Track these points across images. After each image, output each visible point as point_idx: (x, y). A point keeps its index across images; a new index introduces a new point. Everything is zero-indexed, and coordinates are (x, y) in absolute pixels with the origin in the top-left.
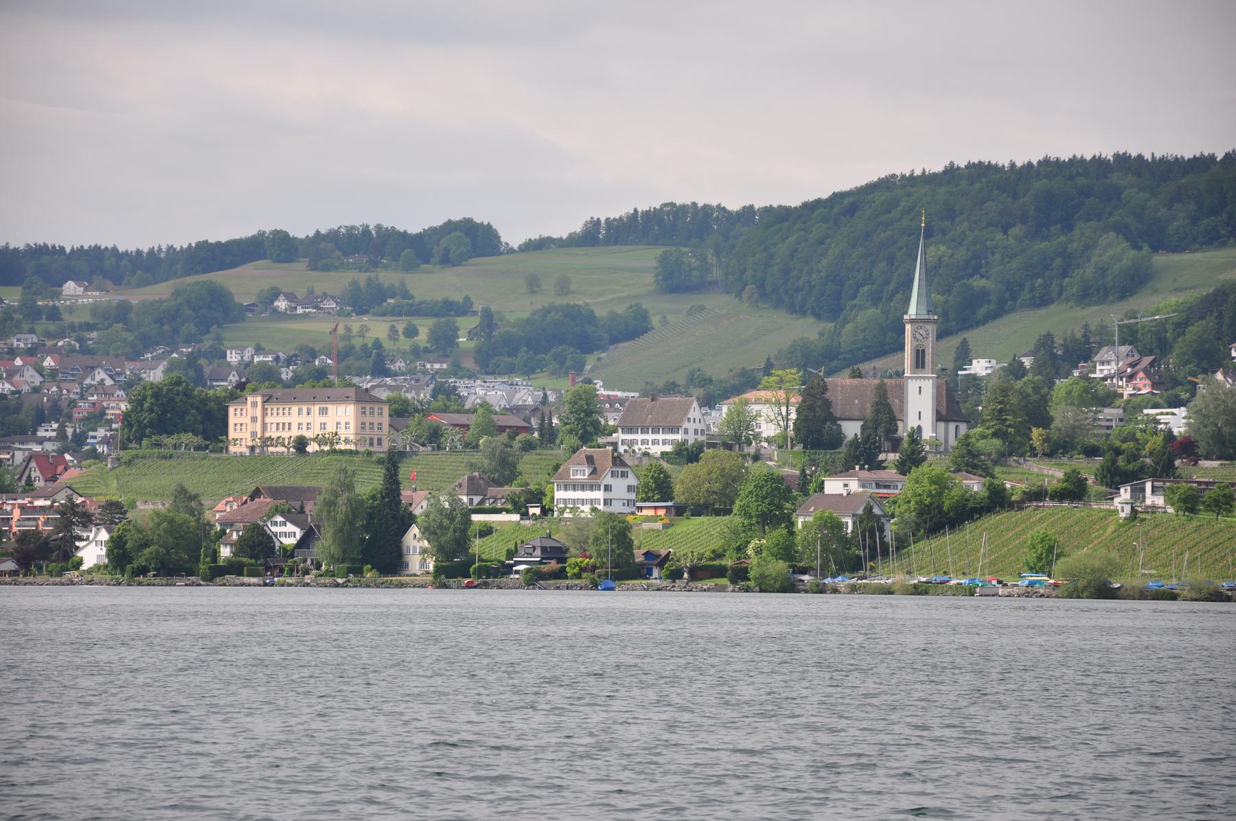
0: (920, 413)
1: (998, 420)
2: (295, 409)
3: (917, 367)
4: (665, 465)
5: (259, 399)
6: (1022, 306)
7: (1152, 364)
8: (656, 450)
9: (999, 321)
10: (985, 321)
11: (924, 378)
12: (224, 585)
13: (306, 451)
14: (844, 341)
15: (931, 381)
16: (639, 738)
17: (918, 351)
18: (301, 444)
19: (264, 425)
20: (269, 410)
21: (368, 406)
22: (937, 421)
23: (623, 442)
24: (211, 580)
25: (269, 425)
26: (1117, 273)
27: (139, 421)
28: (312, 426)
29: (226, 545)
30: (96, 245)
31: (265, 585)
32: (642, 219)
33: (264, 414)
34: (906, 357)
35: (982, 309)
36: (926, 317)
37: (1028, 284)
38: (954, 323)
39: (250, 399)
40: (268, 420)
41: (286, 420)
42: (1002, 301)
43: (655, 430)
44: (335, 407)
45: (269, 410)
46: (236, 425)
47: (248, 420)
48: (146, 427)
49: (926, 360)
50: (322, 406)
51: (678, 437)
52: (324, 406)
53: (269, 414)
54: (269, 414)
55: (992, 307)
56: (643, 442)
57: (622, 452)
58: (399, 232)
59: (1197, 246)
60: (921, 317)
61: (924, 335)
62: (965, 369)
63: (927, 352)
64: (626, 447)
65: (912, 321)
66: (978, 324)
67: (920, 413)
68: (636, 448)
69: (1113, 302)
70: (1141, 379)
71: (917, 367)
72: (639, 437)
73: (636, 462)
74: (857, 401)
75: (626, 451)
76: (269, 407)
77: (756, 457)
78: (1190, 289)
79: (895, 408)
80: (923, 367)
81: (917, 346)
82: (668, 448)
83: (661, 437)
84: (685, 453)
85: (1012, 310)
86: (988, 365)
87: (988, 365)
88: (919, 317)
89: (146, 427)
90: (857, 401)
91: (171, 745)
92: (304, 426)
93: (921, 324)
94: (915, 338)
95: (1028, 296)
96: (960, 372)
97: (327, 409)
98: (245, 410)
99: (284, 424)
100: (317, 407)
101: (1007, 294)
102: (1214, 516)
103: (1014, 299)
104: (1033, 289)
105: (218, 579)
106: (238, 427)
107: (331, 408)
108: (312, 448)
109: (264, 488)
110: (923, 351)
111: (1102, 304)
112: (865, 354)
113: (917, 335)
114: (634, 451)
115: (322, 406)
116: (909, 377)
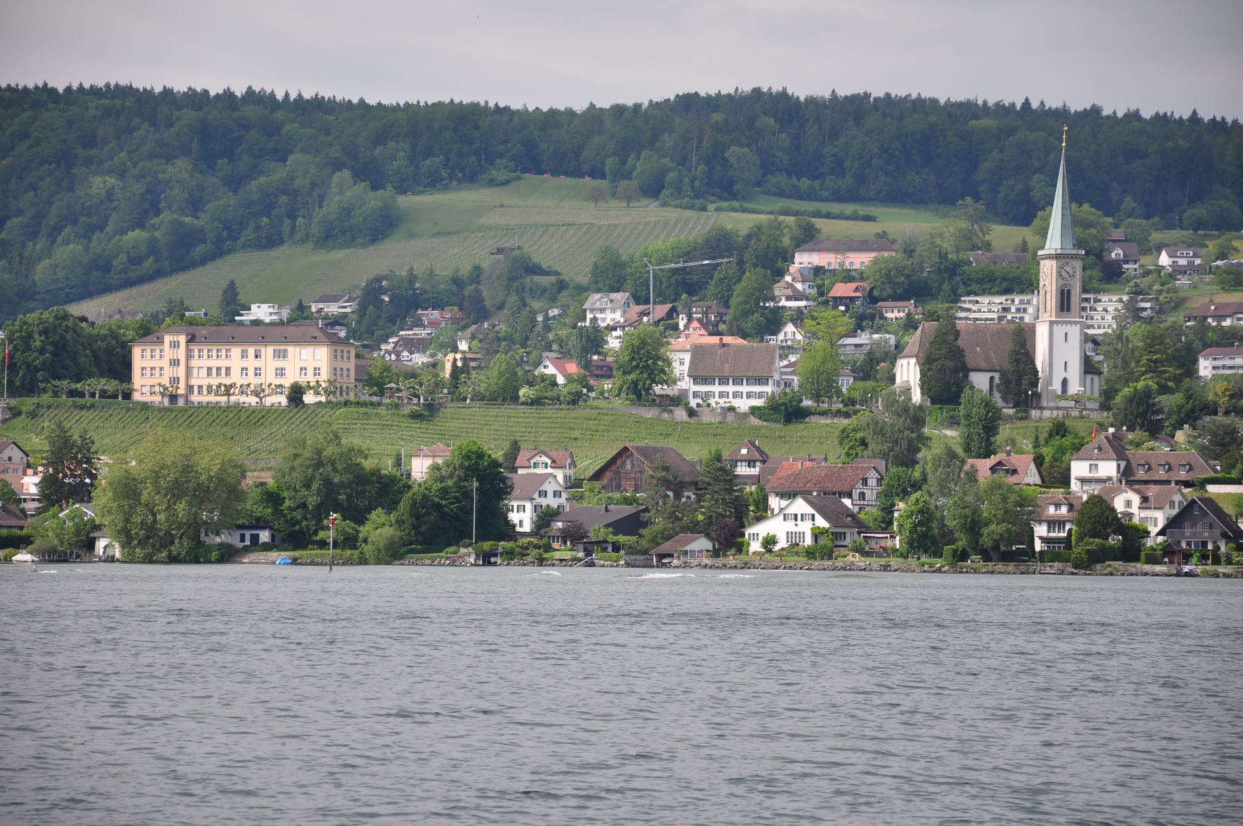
1: (1154, 372)
2: (236, 351)
3: (1062, 310)
4: (755, 421)
5: (182, 339)
6: (244, 246)
8: (743, 405)
9: (219, 262)
10: (203, 262)
11: (1071, 323)
12: (1111, 574)
13: (305, 405)
14: (40, 280)
16: (875, 709)
17: (1062, 291)
18: (296, 394)
19: (189, 369)
20: (196, 351)
21: (339, 349)
23: (695, 395)
24: (1087, 567)
25: (195, 371)
26: (368, 213)
27: (27, 363)
28: (263, 372)
29: (1040, 522)
31: (1178, 574)
33: (189, 356)
35: (198, 249)
36: (1074, 252)
37: (252, 223)
38: (167, 264)
39: (167, 339)
40: (195, 363)
41: (223, 363)
42: (219, 241)
43: (739, 381)
44: (297, 349)
45: (196, 351)
46: (143, 369)
47: (165, 363)
48: (37, 370)
49: (1072, 302)
50: (277, 348)
51: (768, 389)
52: (282, 348)
53: (196, 356)
54: (196, 356)
55: (210, 246)
56: (721, 395)
57: (695, 406)
58: (1080, 112)
59: (421, 188)
61: (1071, 273)
62: (242, 315)
63: (1073, 293)
64: (700, 401)
66: (194, 265)
68: (712, 402)
69: (363, 246)
70: (695, 329)
72: (716, 388)
73: (718, 419)
74: (978, 349)
75: (698, 405)
76: (195, 349)
78: (454, 233)
80: (1069, 310)
82: (759, 402)
83: (744, 389)
84: (783, 408)
85: (229, 252)
86: (271, 310)
87: (271, 310)
89: (37, 370)
90: (978, 349)
91: (479, 741)
92: (251, 372)
94: (1060, 276)
95: (253, 236)
96: (236, 318)
97: (285, 351)
98: (158, 351)
99: (219, 369)
100: (270, 349)
101: (225, 234)
103: (235, 239)
104: (258, 228)
105: (1098, 566)
106: (148, 372)
107: (292, 350)
108: (309, 398)
109: (637, 448)
110: (1069, 291)
111: (349, 247)
112: (68, 294)
113: (1064, 273)
114: (709, 405)
115: (277, 348)
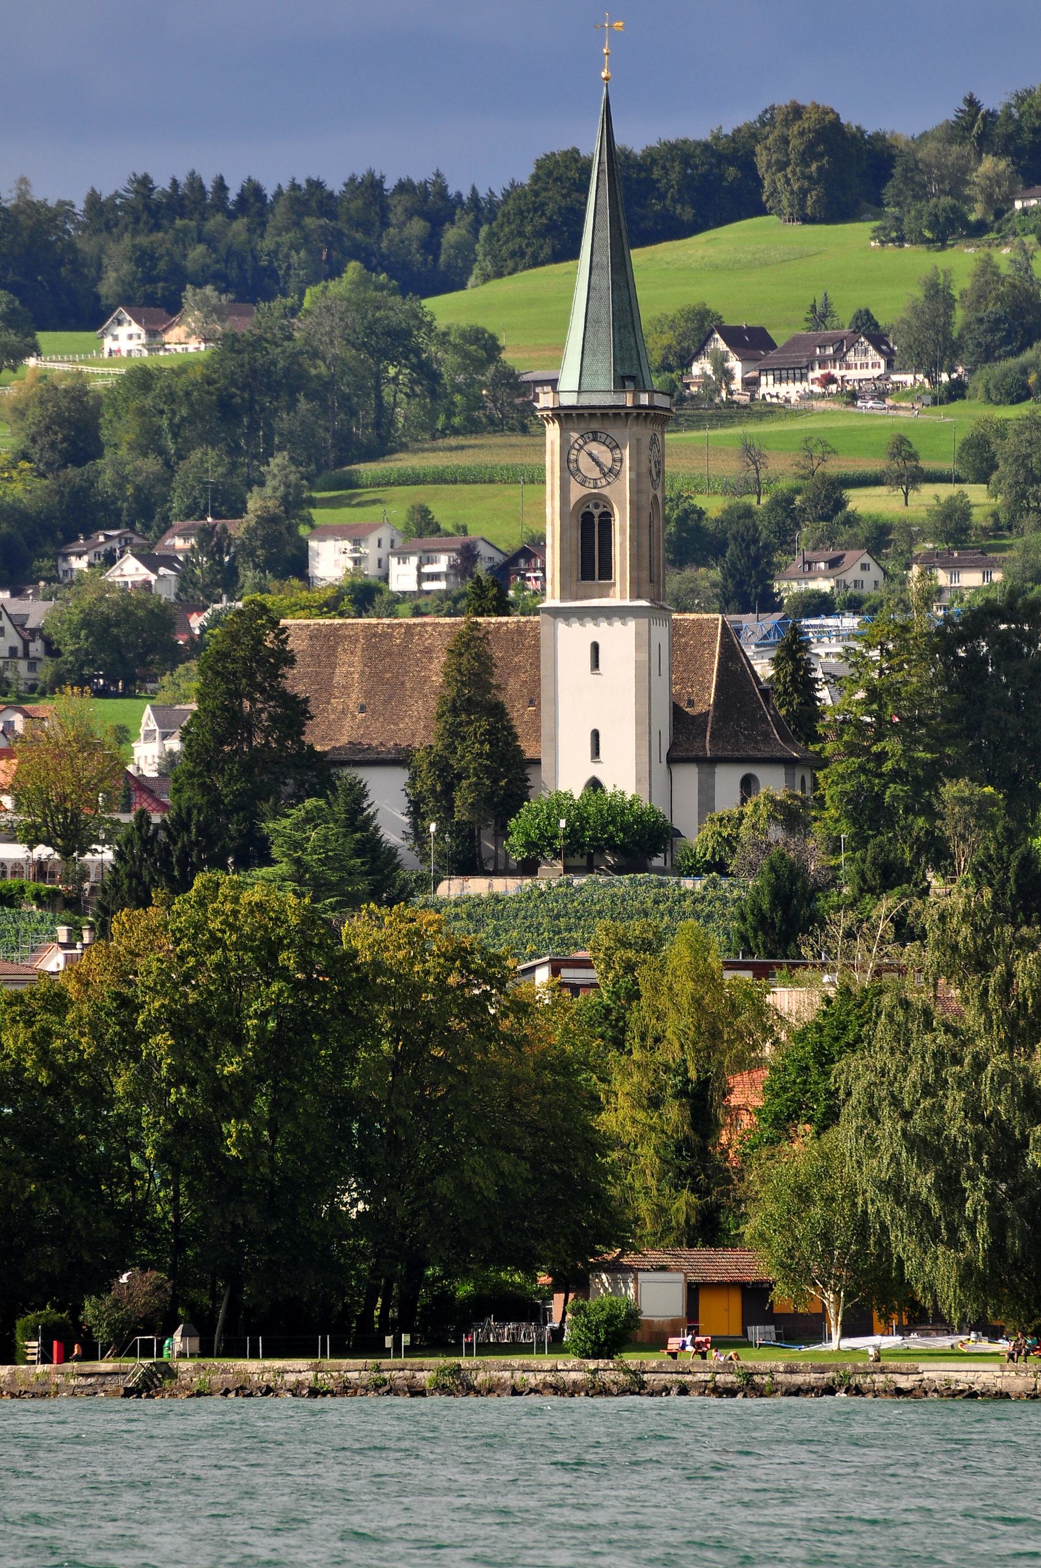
0: (596, 735)
3: (587, 574)
7: (154, 267)
15: (638, 256)
17: (587, 517)
22: (673, 759)
30: (371, 174)
32: (351, 472)
34: (548, 511)
36: (608, 400)
60: (596, 400)
65: (564, 415)
67: (596, 735)
71: (587, 574)
77: (295, 1135)
79: (518, 714)
80: (606, 573)
81: (585, 500)
88: (587, 400)
93: (595, 425)
102: (85, 605)
116: (556, 613)
